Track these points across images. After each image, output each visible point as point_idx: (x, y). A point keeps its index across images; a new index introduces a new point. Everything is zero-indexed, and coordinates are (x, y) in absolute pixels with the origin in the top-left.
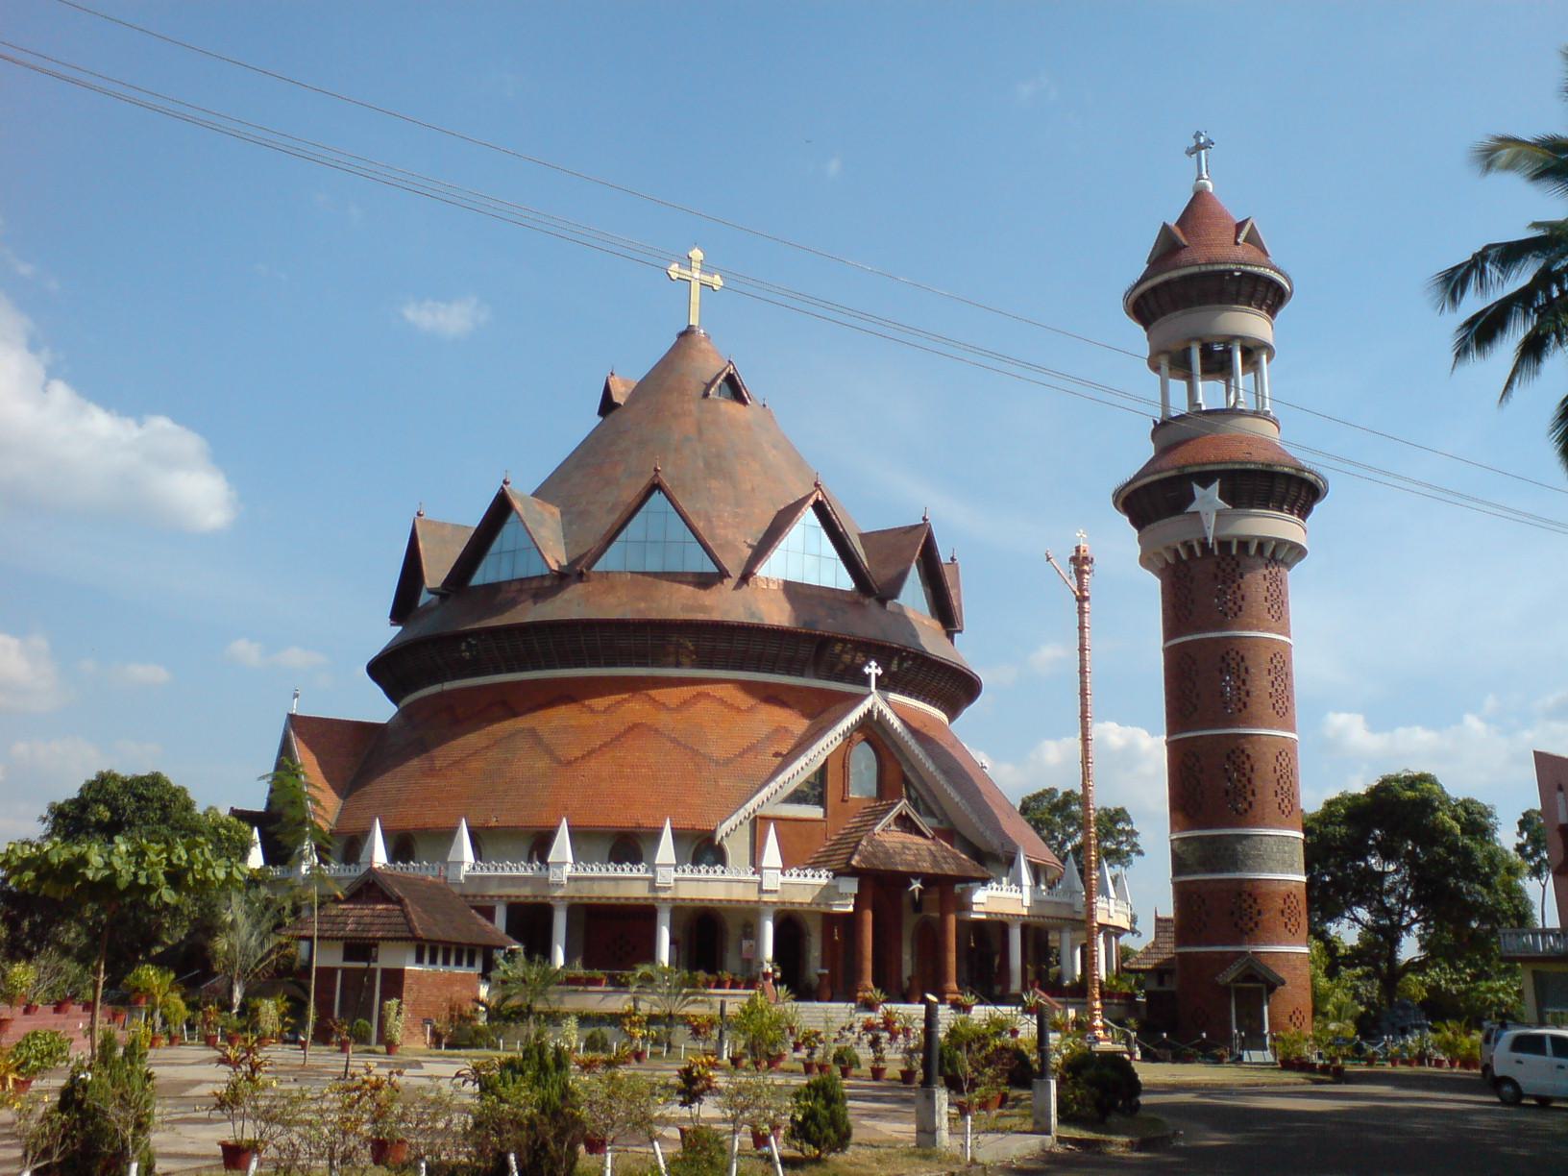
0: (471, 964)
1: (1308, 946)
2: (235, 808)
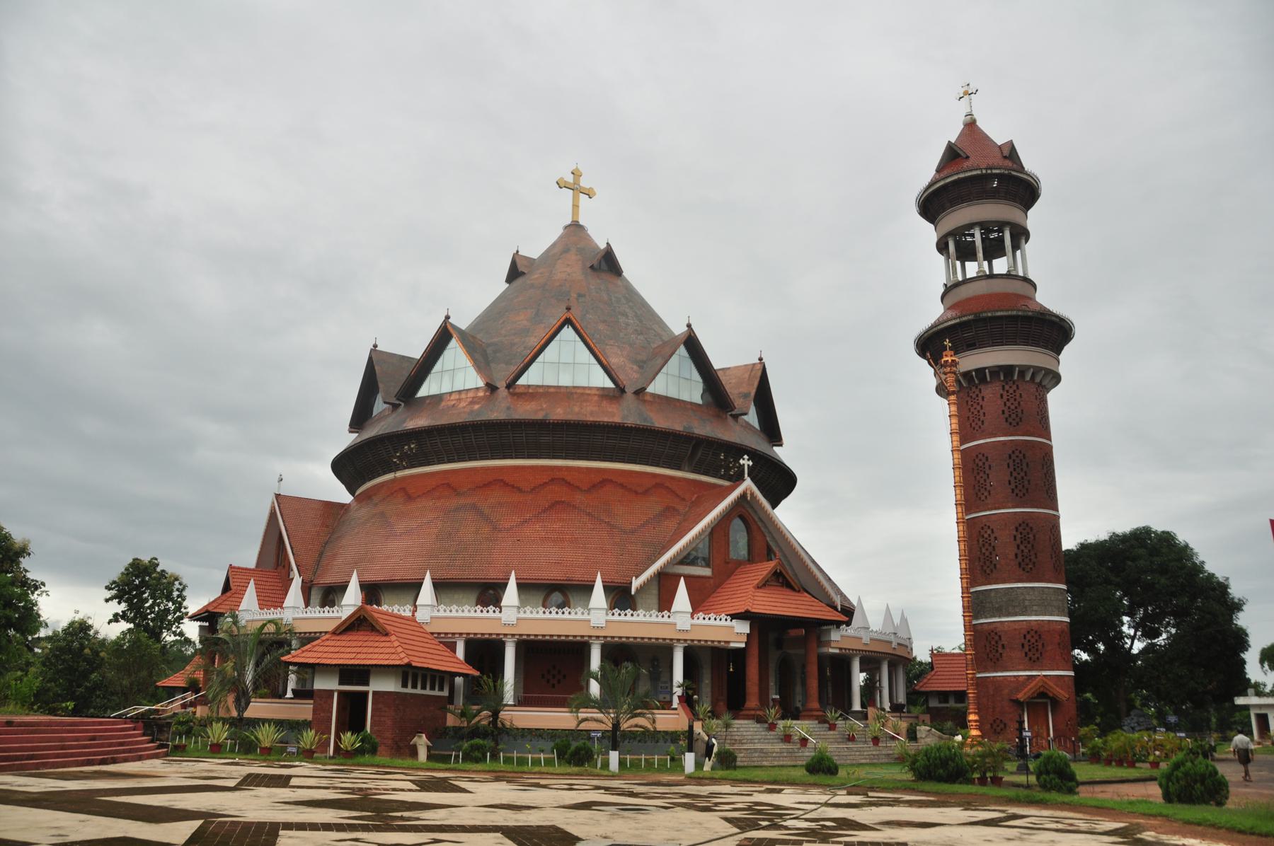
0: (441, 689)
2: (235, 564)
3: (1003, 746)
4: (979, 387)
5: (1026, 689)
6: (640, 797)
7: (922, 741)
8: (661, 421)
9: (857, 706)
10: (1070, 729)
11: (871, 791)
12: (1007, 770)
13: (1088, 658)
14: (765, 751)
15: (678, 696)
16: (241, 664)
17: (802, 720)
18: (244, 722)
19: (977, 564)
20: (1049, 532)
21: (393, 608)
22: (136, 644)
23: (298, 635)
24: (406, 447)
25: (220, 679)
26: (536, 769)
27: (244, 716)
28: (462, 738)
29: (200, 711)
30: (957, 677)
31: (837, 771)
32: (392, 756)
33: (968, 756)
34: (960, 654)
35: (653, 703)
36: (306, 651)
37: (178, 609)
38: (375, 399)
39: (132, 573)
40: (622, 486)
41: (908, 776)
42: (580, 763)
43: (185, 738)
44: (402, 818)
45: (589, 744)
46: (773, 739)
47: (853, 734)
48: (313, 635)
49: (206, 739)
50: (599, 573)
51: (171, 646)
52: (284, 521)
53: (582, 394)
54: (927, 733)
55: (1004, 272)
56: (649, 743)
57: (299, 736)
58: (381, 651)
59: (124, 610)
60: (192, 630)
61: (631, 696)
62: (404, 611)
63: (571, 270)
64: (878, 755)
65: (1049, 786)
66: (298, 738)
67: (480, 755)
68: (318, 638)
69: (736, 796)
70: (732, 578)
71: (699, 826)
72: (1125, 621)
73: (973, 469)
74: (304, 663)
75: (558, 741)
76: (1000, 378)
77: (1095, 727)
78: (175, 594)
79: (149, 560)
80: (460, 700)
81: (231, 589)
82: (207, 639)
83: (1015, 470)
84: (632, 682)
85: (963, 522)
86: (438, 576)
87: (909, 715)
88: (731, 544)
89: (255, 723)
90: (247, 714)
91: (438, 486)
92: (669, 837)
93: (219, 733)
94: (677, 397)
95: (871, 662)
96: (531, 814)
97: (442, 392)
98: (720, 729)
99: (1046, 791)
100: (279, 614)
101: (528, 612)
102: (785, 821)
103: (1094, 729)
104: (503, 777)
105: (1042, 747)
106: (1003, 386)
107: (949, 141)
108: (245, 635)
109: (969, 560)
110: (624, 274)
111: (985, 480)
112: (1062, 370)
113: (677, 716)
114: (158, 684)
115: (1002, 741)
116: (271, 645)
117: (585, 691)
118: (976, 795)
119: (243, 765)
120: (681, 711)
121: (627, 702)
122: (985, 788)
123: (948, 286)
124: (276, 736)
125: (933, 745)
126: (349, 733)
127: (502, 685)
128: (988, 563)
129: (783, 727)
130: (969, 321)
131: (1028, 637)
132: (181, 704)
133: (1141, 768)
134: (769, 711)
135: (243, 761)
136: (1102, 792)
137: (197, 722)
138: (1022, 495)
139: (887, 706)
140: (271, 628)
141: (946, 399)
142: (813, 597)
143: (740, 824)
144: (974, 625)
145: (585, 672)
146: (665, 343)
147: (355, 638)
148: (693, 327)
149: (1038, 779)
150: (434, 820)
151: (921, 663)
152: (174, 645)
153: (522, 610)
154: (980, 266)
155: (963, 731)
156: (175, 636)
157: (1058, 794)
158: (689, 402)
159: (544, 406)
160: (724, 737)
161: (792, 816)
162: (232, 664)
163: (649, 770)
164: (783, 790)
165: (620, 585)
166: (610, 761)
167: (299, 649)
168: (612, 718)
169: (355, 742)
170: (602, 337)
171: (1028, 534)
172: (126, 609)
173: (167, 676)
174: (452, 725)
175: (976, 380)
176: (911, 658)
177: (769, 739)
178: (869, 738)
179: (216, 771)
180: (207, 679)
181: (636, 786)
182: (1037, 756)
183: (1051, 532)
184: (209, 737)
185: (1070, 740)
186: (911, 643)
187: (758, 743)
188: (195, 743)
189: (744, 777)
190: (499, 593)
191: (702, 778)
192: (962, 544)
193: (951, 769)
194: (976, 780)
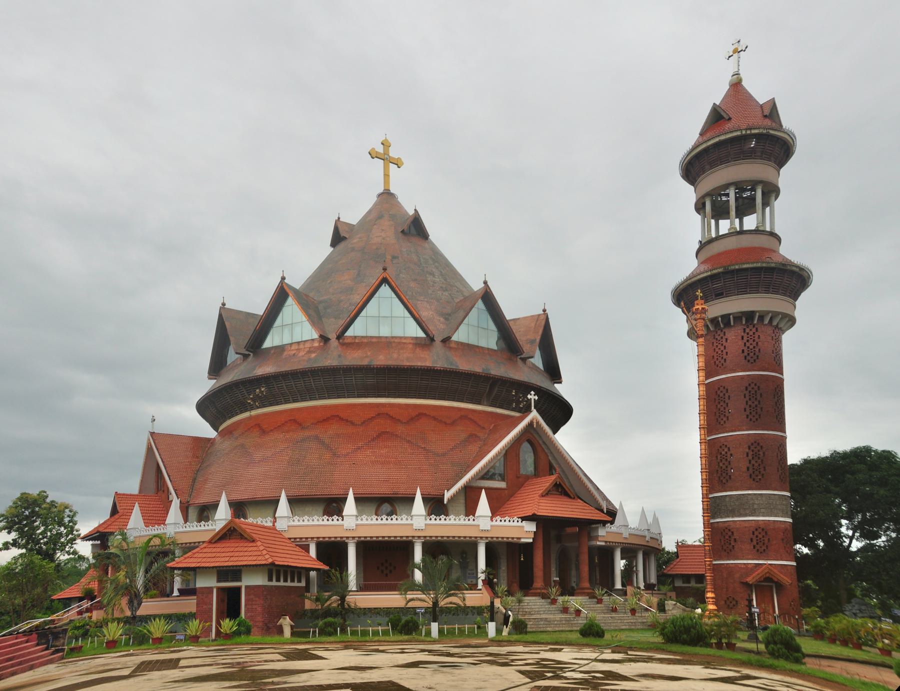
0: (299, 581)
1: (796, 562)
3: (735, 618)
4: (723, 331)
5: (754, 575)
6: (455, 657)
7: (670, 612)
8: (464, 365)
9: (618, 586)
10: (793, 608)
11: (630, 650)
12: (739, 638)
13: (809, 552)
14: (548, 620)
15: (482, 580)
16: (132, 573)
17: (576, 596)
18: (137, 619)
19: (715, 475)
20: (777, 450)
21: (256, 520)
22: (29, 567)
23: (180, 545)
24: (258, 390)
25: (113, 586)
26: (376, 638)
27: (137, 614)
28: (317, 618)
29: (96, 615)
30: (697, 563)
31: (604, 634)
32: (263, 635)
33: (707, 625)
34: (700, 545)
35: (463, 586)
36: (188, 557)
37: (71, 532)
38: (228, 350)
39: (21, 506)
40: (435, 418)
41: (659, 639)
42: (409, 632)
43: (81, 641)
44: (273, 683)
45: (415, 618)
46: (554, 611)
47: (615, 607)
48: (192, 544)
49: (102, 638)
50: (418, 487)
51: (65, 564)
52: (160, 455)
53: (399, 343)
54: (674, 606)
55: (753, 228)
56: (461, 616)
57: (186, 626)
58: (250, 554)
59: (14, 538)
60: (85, 549)
61: (446, 580)
62: (266, 522)
63: (385, 234)
64: (635, 623)
65: (777, 654)
66: (185, 627)
67: (332, 630)
68: (197, 547)
69: (527, 654)
70: (522, 489)
71: (499, 677)
72: (843, 524)
73: (715, 399)
74: (187, 567)
75: (391, 616)
76: (742, 322)
77: (817, 609)
78: (66, 520)
79: (38, 493)
80: (314, 589)
81: (118, 512)
82: (99, 555)
83: (750, 399)
84: (446, 571)
85: (705, 442)
86: (292, 493)
87: (659, 592)
88: (521, 463)
89: (146, 619)
90: (140, 613)
91: (286, 422)
92: (477, 687)
93: (114, 631)
94: (477, 345)
95: (629, 552)
96: (372, 673)
97: (284, 343)
98: (514, 604)
99: (775, 659)
100: (162, 530)
101: (364, 519)
102: (565, 673)
103: (816, 611)
104: (351, 646)
105: (769, 621)
106: (744, 329)
107: (714, 104)
108: (133, 549)
109: (708, 472)
110: (430, 237)
111: (725, 408)
112: (797, 314)
113: (482, 595)
114: (52, 598)
115: (735, 615)
116: (158, 555)
117: (411, 578)
118: (714, 657)
119: (137, 655)
120: (484, 591)
121: (443, 585)
122: (722, 651)
123: (703, 243)
124: (166, 627)
125: (678, 616)
126: (227, 619)
127: (347, 576)
128: (724, 475)
129: (562, 602)
130: (719, 273)
131: (756, 533)
132: (77, 612)
133: (869, 652)
134: (551, 590)
135: (137, 652)
136: (829, 666)
137: (93, 625)
138: (755, 420)
139: (642, 585)
140: (157, 541)
141: (696, 341)
142: (585, 502)
143: (531, 675)
144: (711, 523)
145: (411, 564)
146: (466, 298)
147: (228, 545)
148: (488, 283)
149: (767, 647)
150: (298, 682)
151: (668, 553)
152: (68, 563)
153: (359, 518)
154: (732, 223)
155: (702, 606)
156: (69, 555)
157: (785, 662)
158: (476, 346)
159: (369, 354)
160: (517, 610)
161: (570, 669)
162: (124, 573)
163: (461, 636)
164: (563, 649)
165: (435, 496)
166: (432, 631)
167: (182, 556)
168: (432, 598)
169: (233, 626)
170: (414, 294)
171: (759, 451)
172: (17, 537)
173: (62, 590)
174: (309, 608)
175: (721, 324)
176: (661, 549)
177: (552, 611)
178: (628, 609)
179: (112, 663)
180: (101, 589)
181: (452, 648)
182: (765, 629)
183: (779, 450)
184: (105, 636)
185: (794, 618)
186: (661, 537)
187: (543, 614)
188: (91, 643)
189: (533, 639)
190: (340, 505)
191: (502, 641)
192: (704, 460)
193: (693, 635)
194: (714, 644)
